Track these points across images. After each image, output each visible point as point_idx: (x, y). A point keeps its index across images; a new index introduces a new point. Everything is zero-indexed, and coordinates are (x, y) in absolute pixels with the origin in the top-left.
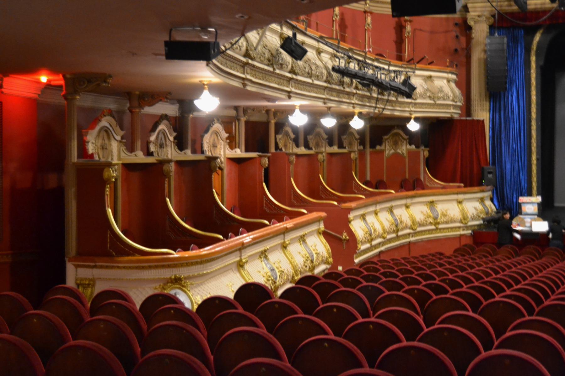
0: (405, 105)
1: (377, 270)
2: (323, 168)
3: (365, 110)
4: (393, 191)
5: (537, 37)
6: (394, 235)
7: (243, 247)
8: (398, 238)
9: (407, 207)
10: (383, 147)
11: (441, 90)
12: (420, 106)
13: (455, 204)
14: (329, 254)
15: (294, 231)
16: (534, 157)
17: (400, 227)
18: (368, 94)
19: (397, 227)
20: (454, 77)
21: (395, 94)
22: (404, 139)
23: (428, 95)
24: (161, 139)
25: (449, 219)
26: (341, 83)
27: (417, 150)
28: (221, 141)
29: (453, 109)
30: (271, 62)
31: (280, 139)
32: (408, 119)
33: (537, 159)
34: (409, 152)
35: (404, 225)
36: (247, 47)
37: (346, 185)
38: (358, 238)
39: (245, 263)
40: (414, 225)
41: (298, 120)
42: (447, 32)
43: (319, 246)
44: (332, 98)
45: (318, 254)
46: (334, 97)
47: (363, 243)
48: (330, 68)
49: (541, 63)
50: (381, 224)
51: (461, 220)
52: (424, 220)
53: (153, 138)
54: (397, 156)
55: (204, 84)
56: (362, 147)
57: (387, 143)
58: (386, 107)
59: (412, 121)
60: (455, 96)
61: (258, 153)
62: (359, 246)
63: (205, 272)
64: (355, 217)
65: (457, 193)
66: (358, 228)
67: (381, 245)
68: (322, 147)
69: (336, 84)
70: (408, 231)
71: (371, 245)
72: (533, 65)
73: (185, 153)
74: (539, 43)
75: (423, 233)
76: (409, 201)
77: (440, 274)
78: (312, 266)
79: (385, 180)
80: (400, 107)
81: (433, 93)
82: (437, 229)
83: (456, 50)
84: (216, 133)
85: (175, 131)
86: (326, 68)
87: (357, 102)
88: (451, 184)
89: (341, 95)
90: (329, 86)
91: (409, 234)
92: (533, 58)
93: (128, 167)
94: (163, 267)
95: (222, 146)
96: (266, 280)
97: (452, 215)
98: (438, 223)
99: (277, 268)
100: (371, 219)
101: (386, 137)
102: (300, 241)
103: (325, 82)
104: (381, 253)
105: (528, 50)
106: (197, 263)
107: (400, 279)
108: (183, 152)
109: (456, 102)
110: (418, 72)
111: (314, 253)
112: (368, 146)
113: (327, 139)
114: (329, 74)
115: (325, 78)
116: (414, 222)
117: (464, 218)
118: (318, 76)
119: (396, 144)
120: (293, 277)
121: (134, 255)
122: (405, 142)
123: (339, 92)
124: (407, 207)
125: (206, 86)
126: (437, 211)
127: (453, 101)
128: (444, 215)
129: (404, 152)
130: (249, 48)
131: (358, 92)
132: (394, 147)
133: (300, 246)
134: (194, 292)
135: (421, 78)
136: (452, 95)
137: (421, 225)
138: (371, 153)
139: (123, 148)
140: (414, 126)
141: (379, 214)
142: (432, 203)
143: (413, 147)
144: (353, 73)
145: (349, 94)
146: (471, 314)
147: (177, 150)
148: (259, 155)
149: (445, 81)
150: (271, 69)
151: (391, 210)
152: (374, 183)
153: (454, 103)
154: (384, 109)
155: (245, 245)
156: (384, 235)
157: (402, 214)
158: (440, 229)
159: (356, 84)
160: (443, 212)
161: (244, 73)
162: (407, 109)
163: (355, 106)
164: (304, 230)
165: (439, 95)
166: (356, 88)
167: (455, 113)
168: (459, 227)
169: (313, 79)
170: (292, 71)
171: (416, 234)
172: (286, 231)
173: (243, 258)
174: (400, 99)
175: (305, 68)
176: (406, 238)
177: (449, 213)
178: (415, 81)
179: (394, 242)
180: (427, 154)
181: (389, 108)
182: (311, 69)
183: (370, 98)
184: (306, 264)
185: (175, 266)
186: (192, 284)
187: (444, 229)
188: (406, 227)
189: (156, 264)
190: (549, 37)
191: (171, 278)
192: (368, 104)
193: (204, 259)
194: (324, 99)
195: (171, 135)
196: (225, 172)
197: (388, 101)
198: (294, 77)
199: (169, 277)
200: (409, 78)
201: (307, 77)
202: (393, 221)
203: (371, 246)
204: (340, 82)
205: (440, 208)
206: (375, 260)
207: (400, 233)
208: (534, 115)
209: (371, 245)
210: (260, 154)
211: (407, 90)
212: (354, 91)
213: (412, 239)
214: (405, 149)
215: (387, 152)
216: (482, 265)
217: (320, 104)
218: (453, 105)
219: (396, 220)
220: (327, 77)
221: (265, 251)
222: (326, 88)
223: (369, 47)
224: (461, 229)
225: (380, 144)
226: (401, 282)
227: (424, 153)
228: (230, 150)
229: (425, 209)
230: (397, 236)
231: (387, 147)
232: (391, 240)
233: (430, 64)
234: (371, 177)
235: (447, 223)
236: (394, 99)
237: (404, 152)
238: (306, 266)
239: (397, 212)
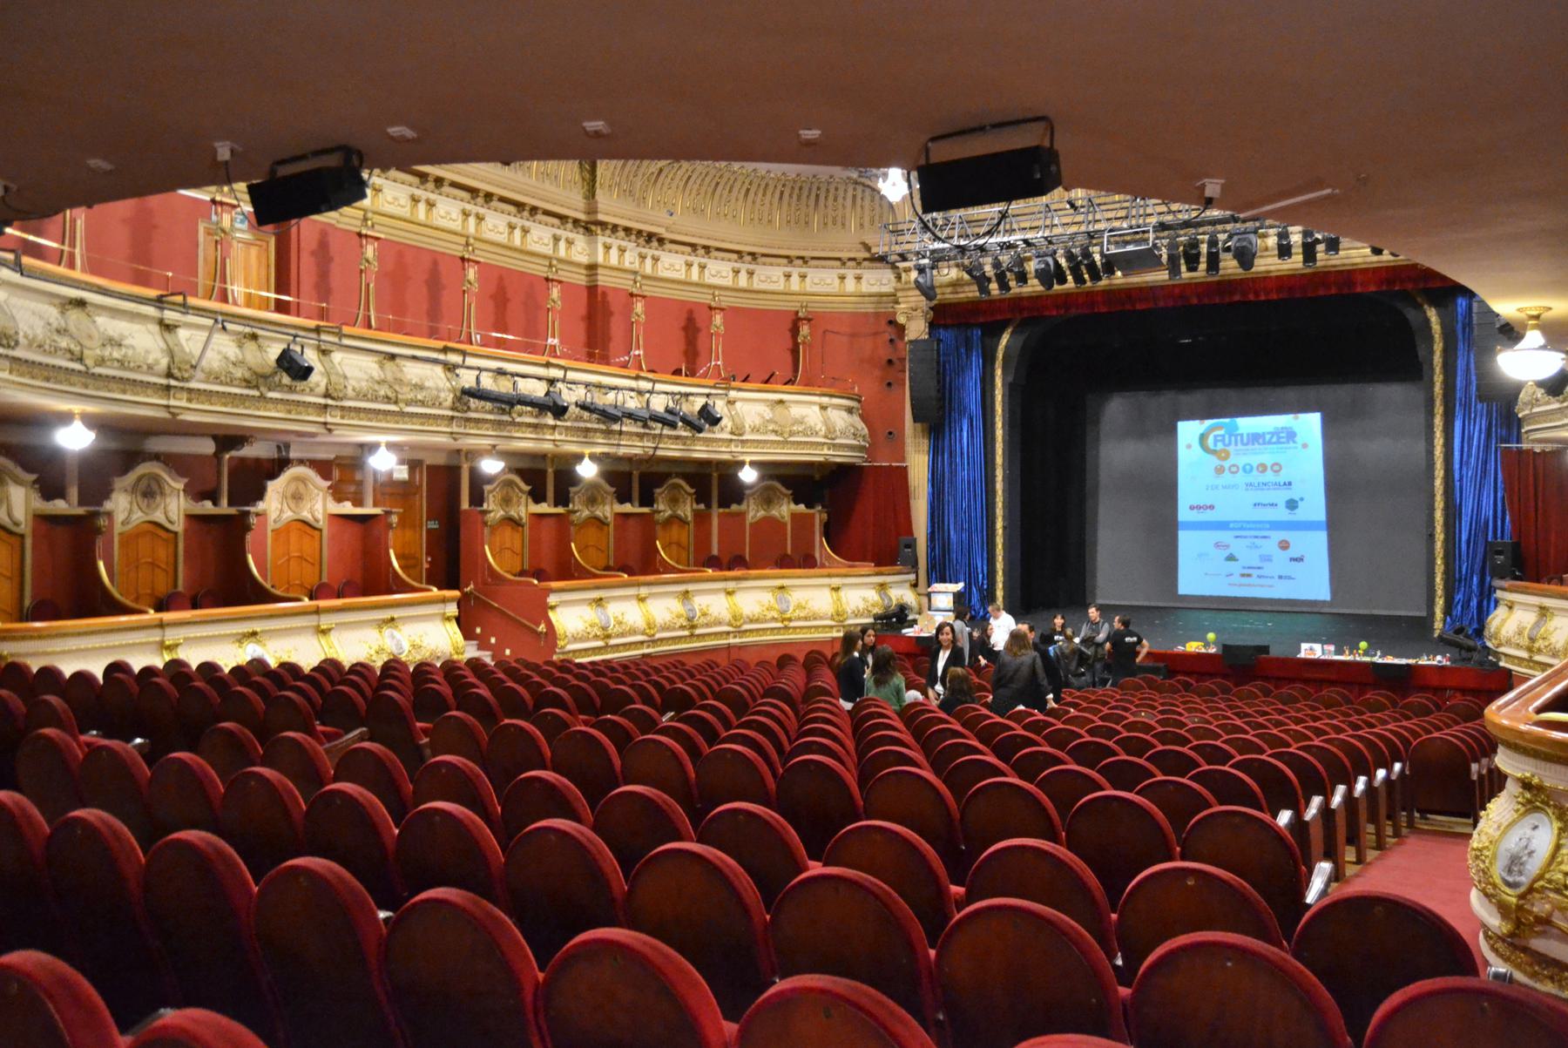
3: (598, 450)
5: (1005, 338)
10: (743, 507)
16: (999, 524)
33: (1004, 528)
34: (794, 516)
42: (876, 334)
49: (1010, 379)
62: (560, 643)
72: (999, 382)
74: (1007, 347)
77: (1275, 742)
83: (890, 362)
92: (999, 372)
93: (43, 520)
97: (631, 622)
101: (658, 491)
103: (453, 409)
105: (989, 359)
114: (457, 399)
117: (839, 615)
138: (720, 516)
146: (927, 774)
149: (817, 408)
150: (256, 393)
152: (725, 561)
170: (327, 395)
171: (654, 642)
177: (810, 605)
187: (751, 631)
190: (1021, 339)
196: (325, 533)
203: (607, 646)
208: (999, 460)
213: (732, 641)
215: (751, 514)
216: (1344, 731)
222: (452, 418)
225: (739, 502)
226: (1193, 754)
227: (819, 515)
233: (745, 380)
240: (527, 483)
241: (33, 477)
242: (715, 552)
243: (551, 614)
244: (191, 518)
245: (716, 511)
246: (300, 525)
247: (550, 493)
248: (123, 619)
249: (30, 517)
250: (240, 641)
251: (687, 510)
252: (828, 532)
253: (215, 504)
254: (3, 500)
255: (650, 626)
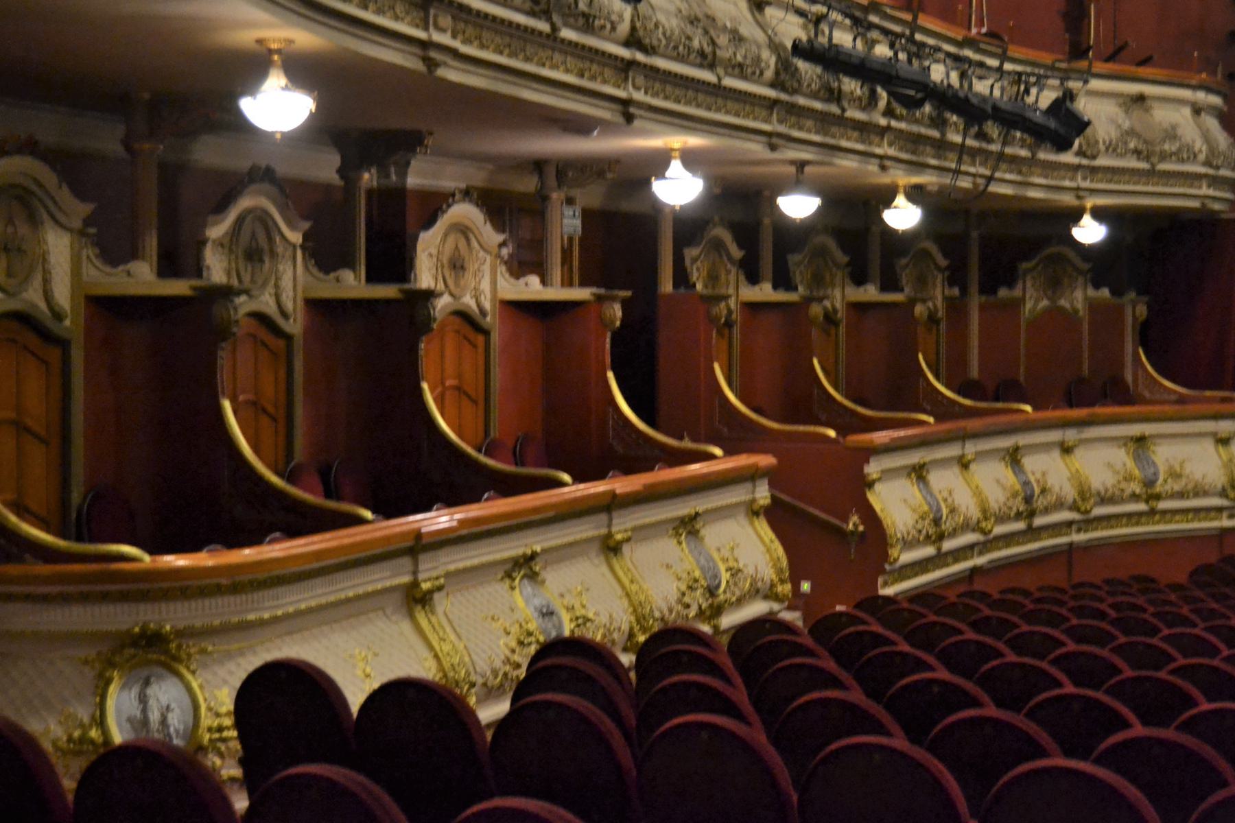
0: (1062, 173)
1: (1102, 615)
2: (837, 344)
3: (926, 179)
4: (1028, 408)
6: (1020, 525)
7: (419, 546)
8: (1032, 533)
9: (1066, 450)
10: (1017, 292)
11: (1171, 134)
12: (1109, 176)
13: (1209, 445)
14: (779, 571)
15: (669, 502)
17: (1040, 503)
18: (935, 134)
19: (1029, 503)
20: (1215, 100)
21: (1029, 140)
22: (1081, 272)
23: (1132, 145)
24: (254, 236)
25: (1190, 487)
26: (835, 96)
27: (1117, 301)
28: (482, 253)
29: (1209, 186)
30: (543, 6)
31: (694, 260)
32: (1075, 216)
34: (1093, 306)
35: (1051, 498)
36: (632, 21)
37: (897, 392)
38: (890, 531)
39: (430, 592)
40: (1083, 500)
41: (678, 189)
43: (745, 550)
44: (796, 134)
45: (735, 572)
46: (809, 131)
47: (908, 544)
48: (789, 45)
50: (977, 493)
51: (1224, 489)
52: (1114, 486)
53: (217, 230)
54: (1055, 313)
55: (271, 52)
56: (956, 291)
57: (1029, 284)
58: (997, 175)
59: (1087, 220)
60: (1212, 150)
61: (594, 290)
62: (894, 552)
63: (251, 617)
64: (887, 474)
65: (1216, 417)
66: (895, 502)
67: (976, 550)
68: (833, 286)
69: (814, 96)
70: (1066, 515)
71: (939, 549)
73: (338, 280)
75: (1113, 522)
76: (1071, 435)
78: (711, 606)
79: (1022, 379)
80: (1046, 177)
81: (1146, 142)
82: (1153, 512)
84: (463, 230)
85: (305, 217)
86: (775, 47)
87: (891, 152)
88: (1208, 393)
89: (834, 129)
90: (784, 97)
91: (1069, 524)
94: (105, 597)
95: (486, 268)
96: (513, 644)
97: (1198, 476)
98: (1158, 497)
99: (570, 609)
100: (944, 481)
101: (1025, 265)
102: (678, 535)
103: (773, 85)
104: (974, 571)
106: (218, 591)
107: (1164, 639)
108: (332, 275)
109: (1217, 168)
110: (1095, 84)
111: (722, 568)
112: (974, 288)
113: (848, 265)
114: (784, 66)
115: (769, 74)
116: (1084, 493)
118: (740, 66)
119: (1054, 285)
120: (631, 635)
121: (19, 560)
122: (1081, 280)
123: (824, 121)
124: (1066, 450)
125: (276, 57)
126: (1154, 463)
127: (1207, 163)
128: (1175, 475)
129: (1080, 305)
130: (638, 25)
131: (894, 123)
132: (1049, 293)
133: (678, 549)
134: (210, 677)
135: (1112, 101)
136: (1204, 148)
137: (1104, 500)
138: (982, 308)
139: (90, 252)
140: (1090, 232)
141: (973, 467)
142: (1141, 440)
143: (1105, 292)
144: (854, 60)
145: (864, 129)
147: (315, 271)
148: (594, 295)
149: (1187, 111)
150: (543, 26)
151: (1014, 458)
153: (1211, 171)
154: (990, 179)
155: (424, 541)
156: (983, 524)
157: (1051, 470)
158: (1164, 512)
159: (889, 103)
160: (1171, 467)
161: (426, 28)
162: (1067, 183)
163: (888, 163)
164: (693, 503)
165: (1166, 147)
166: (889, 112)
167: (1214, 198)
168: (1220, 510)
169: (721, 71)
170: (633, 41)
171: (1089, 523)
172: (611, 505)
173: (421, 576)
174: (1042, 155)
175: (689, 38)
176: (1060, 535)
178: (1085, 106)
179: (1019, 544)
180: (1142, 311)
181: (1008, 176)
182: (713, 42)
183: (941, 146)
184: (687, 599)
185: (144, 597)
186: (203, 651)
188: (1059, 505)
189: (85, 588)
191: (129, 632)
192: (933, 162)
193: (246, 578)
194: (769, 135)
195: (292, 226)
196: (495, 337)
197: (1001, 157)
198: (640, 57)
199: (124, 627)
200: (1069, 96)
201: (701, 66)
202: (1018, 487)
204: (830, 90)
205: (1164, 455)
206: (952, 595)
207: (1039, 521)
209: (939, 549)
210: (602, 291)
211: (1064, 126)
212: (883, 122)
214: (1079, 297)
217: (755, 148)
218: (1206, 176)
219: (1026, 483)
220: (777, 73)
221: (533, 557)
222: (775, 102)
223: (980, 24)
224: (1225, 514)
225: (1011, 284)
227: (1136, 309)
228: (512, 280)
229: (1121, 457)
230: (1030, 527)
231: (1030, 292)
232: (1008, 539)
234: (981, 371)
235: (1181, 495)
236: (1024, 153)
237: (1080, 305)
238: (688, 606)
239: (1033, 464)
240: (946, 255)
241: (85, 209)
242: (974, 373)
243: (872, 497)
244: (318, 307)
245: (975, 300)
246: (458, 320)
247: (875, 267)
248: (276, 550)
249: (300, 303)
250: (509, 576)
251: (939, 294)
252: (1145, 336)
253: (544, 282)
254: (23, 259)
255: (1084, 493)
